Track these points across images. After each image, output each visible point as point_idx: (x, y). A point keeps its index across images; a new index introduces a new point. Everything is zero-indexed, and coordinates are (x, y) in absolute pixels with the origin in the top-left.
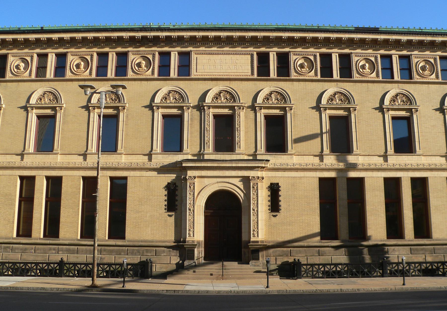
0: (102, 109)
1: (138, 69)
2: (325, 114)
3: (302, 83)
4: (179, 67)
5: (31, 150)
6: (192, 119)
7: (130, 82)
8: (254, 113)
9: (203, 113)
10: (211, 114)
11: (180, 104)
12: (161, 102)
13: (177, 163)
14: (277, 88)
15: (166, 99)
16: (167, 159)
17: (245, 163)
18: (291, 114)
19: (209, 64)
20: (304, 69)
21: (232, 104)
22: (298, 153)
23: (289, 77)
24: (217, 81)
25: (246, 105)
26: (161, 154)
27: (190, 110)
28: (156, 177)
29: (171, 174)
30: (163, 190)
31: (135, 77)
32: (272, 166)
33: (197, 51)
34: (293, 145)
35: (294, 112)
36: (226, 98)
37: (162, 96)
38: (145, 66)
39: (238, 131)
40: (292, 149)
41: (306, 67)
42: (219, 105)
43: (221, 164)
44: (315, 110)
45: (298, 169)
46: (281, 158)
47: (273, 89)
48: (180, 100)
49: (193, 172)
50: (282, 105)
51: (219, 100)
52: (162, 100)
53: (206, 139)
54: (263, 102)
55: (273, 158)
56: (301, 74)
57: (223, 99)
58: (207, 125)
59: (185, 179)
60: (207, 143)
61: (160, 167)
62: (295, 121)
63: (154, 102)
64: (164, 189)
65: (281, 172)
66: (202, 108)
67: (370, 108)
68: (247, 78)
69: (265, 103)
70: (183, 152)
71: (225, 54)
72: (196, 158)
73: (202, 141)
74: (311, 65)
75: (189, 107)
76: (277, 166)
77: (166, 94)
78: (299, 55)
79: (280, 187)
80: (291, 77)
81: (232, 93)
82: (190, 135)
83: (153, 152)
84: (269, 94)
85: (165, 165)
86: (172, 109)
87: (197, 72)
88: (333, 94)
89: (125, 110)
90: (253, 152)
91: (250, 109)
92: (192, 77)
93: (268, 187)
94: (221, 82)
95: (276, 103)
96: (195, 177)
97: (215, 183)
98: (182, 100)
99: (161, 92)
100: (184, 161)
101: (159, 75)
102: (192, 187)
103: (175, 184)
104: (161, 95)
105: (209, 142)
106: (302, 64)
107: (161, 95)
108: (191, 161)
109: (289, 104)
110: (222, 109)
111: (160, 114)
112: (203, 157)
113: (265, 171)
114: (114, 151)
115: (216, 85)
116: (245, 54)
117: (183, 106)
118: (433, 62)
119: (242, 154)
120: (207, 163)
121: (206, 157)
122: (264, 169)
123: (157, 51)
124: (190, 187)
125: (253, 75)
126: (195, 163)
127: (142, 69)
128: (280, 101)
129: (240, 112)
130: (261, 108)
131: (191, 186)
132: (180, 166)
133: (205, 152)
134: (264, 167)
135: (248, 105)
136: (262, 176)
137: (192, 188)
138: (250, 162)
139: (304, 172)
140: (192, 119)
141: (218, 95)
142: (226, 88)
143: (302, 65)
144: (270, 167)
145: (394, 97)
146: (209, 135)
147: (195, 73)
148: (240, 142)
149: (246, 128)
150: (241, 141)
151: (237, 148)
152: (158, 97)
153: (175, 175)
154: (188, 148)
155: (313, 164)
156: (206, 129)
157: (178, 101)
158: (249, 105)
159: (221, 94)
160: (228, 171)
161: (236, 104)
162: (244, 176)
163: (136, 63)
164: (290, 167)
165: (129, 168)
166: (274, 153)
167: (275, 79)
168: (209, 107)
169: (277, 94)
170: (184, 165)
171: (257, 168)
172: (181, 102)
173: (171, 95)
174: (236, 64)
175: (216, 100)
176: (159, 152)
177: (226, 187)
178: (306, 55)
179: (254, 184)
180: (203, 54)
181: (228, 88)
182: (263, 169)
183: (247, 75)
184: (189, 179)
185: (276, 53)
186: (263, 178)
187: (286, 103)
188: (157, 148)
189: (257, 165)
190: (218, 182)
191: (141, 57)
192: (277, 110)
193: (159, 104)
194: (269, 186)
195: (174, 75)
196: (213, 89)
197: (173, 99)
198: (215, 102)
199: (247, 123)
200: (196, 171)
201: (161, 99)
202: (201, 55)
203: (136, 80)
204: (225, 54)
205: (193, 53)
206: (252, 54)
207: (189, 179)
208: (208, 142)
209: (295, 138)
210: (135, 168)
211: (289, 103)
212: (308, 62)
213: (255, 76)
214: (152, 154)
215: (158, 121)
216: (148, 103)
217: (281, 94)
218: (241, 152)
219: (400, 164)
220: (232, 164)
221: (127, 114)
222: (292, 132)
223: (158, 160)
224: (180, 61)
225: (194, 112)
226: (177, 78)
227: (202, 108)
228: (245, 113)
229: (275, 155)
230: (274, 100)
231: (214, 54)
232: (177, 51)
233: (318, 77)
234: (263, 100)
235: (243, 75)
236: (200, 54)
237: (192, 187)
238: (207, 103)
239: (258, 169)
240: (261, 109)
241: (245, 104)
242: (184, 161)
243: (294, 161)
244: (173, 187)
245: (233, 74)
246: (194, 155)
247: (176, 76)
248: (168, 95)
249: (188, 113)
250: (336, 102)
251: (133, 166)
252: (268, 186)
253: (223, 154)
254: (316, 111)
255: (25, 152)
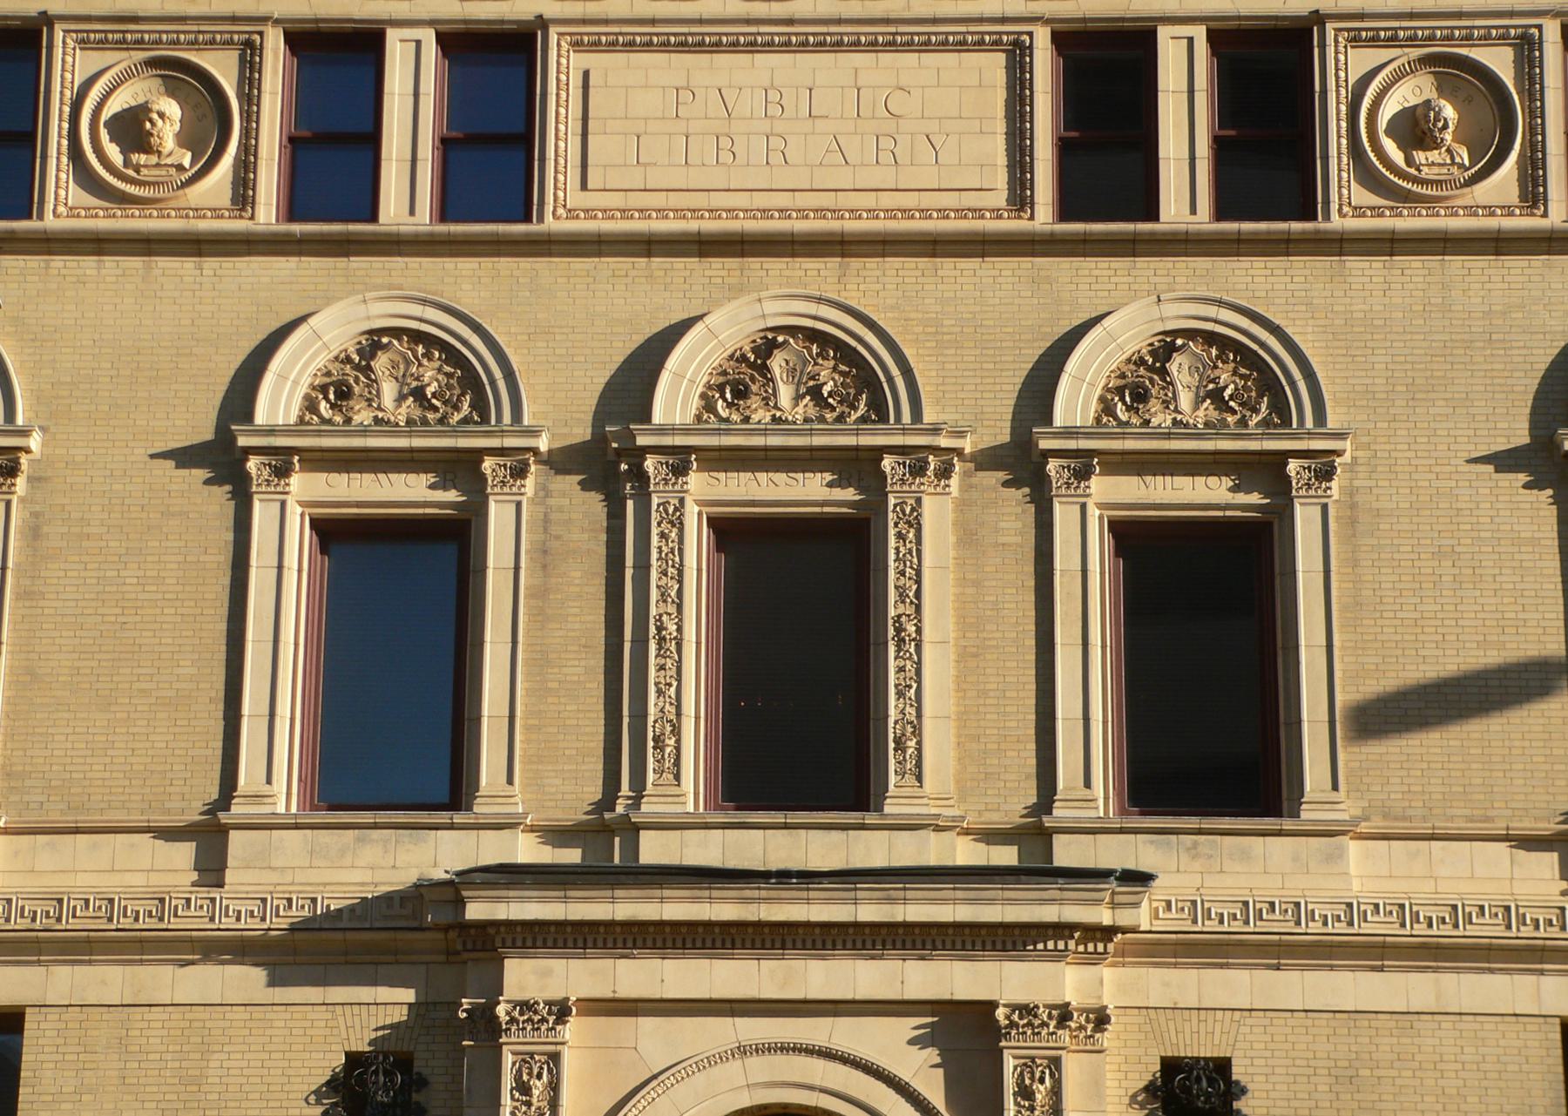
0: (1356, 483)
1: (127, 163)
2: (513, 506)
3: (1415, 265)
4: (446, 145)
5: (284, 796)
6: (545, 552)
7: (58, 262)
8: (1032, 508)
9: (630, 504)
10: (692, 511)
11: (455, 433)
12: (301, 421)
13: (421, 894)
14: (1212, 311)
15: (344, 393)
16: (348, 861)
17: (960, 894)
18: (1325, 507)
19: (681, 126)
20: (1434, 156)
21: (857, 432)
22: (1385, 816)
23: (1315, 218)
24: (742, 255)
25: (968, 445)
26: (297, 827)
27: (530, 483)
28: (258, 1013)
29: (374, 983)
30: (308, 1111)
31: (103, 224)
32: (1173, 922)
33: (584, 22)
34: (1341, 756)
35: (1350, 492)
36: (815, 393)
37: (311, 369)
38: (178, 135)
39: (900, 642)
40: (1335, 787)
41: (1448, 137)
42: (758, 441)
43: (763, 907)
44: (1523, 478)
45: (1384, 946)
46: (1245, 856)
47: (1177, 315)
48: (457, 408)
49: (548, 973)
50: (1249, 437)
51: (754, 402)
52: (311, 406)
53: (652, 711)
54: (1098, 420)
55: (1184, 858)
56: (1406, 197)
57: (785, 394)
58: (664, 597)
59: (486, 1027)
60: (659, 743)
61: (293, 929)
62: (1355, 563)
63: (248, 415)
64: (318, 1102)
65: (1243, 975)
66: (624, 467)
67: (1461, 462)
68: (976, 234)
69: (1121, 424)
70: (469, 808)
71: (805, 44)
72: (572, 856)
73: (626, 720)
74: (1486, 113)
75: (526, 464)
76: (1212, 925)
77: (348, 360)
78: (1394, 38)
79: (1244, 1091)
80: (1327, 217)
81: (1261, 352)
82: (527, 674)
83: (235, 809)
84: (1151, 353)
85: (328, 914)
86: (393, 477)
87: (584, 186)
88: (1153, 353)
89: (21, 482)
90: (199, 806)
91: (1002, 476)
92: (552, 223)
93: (1146, 1089)
94: (776, 266)
95: (1206, 424)
96: (561, 1011)
97: (722, 1058)
98: (1264, 407)
99: (307, 344)
100: (478, 878)
101: (294, 208)
102: (538, 1087)
103: (404, 1063)
104: (306, 365)
105: (677, 731)
106: (1419, 111)
107: (306, 365)
108: (528, 879)
109: (1311, 435)
110: (780, 477)
111: (294, 512)
112: (633, 848)
113: (1113, 965)
114: (446, 800)
115: (736, 291)
116: (964, 43)
117: (480, 453)
118: (1507, 77)
119: (938, 829)
120: (658, 893)
121: (654, 849)
122: (1111, 947)
123: (277, 22)
124: (523, 1088)
125: (1022, 209)
126: (566, 899)
127: (154, 159)
128: (1234, 412)
129: (919, 501)
130: (1083, 466)
131: (534, 1082)
132: (446, 917)
133: (644, 808)
134: (1108, 933)
135: (981, 447)
136: (1092, 1002)
137: (536, 1092)
138: (993, 891)
139: (1435, 970)
140: (543, 553)
141: (752, 366)
142: (812, 308)
143: (1416, 123)
144: (1159, 926)
145: (1141, 362)
146: (679, 680)
147: (576, 198)
148: (918, 731)
149: (969, 621)
150: (928, 725)
151: (892, 779)
152: (282, 377)
153: (409, 995)
154: (510, 781)
155: (1508, 909)
156: (653, 630)
157: (436, 409)
158: (988, 441)
159: (769, 355)
160: (823, 958)
161: (488, 434)
162: (947, 996)
163: (106, 114)
164: (1315, 927)
165: (38, 941)
166: (1192, 822)
167: (1198, 233)
168: (680, 461)
169: (1214, 352)
170: (476, 911)
171: (1056, 939)
172: (466, 421)
173: (381, 363)
174: (890, 126)
175: (730, 405)
176: (281, 809)
177: (811, 1088)
178: (1450, 38)
179: (1029, 1064)
180: (632, 44)
181: (1212, 311)
182: (1100, 948)
183: (978, 213)
184: (513, 1020)
185: (1209, 31)
186: (1101, 1020)
187: (1287, 422)
188: (269, 782)
189: (1048, 914)
190: (743, 1051)
191: (152, 63)
192: (1213, 480)
193: (287, 431)
194: (1152, 1083)
195: (412, 212)
196: (707, 320)
197: (401, 398)
198: (727, 420)
199: (977, 584)
200: (575, 964)
201: (307, 397)
202: (620, 58)
203: (204, 247)
204: (805, 44)
205: (553, 38)
206: (1017, 44)
207: (513, 1020)
208: (909, 729)
209: (1359, 697)
210: (88, 941)
211: (1309, 423)
212: (1469, 100)
213: (1043, 216)
214: (222, 831)
215: (280, 567)
216: (999, 432)
217: (1246, 358)
218: (924, 810)
219: (1194, 903)
220: (856, 901)
221: (35, 515)
222: (1336, 653)
223: (274, 877)
224: (457, 99)
225: (563, 494)
226: (431, 234)
227: (624, 467)
228: (962, 505)
229: (1200, 832)
230: (1185, 400)
231: (598, 43)
232: (430, 23)
233: (1545, 215)
234: (1102, 399)
235: (943, 213)
236: (612, 47)
237: (538, 1087)
238: (662, 430)
239: (1061, 945)
240: (1083, 474)
241: (960, 434)
242: (478, 878)
243: (1356, 886)
244: (387, 1091)
245: (868, 200)
246: (556, 835)
247: (424, 220)
248: (357, 367)
249: (519, 504)
250: (1176, 411)
251: (74, 923)
252: (1142, 1084)
253: (786, 826)
254: (1527, 486)
255: (238, 809)
